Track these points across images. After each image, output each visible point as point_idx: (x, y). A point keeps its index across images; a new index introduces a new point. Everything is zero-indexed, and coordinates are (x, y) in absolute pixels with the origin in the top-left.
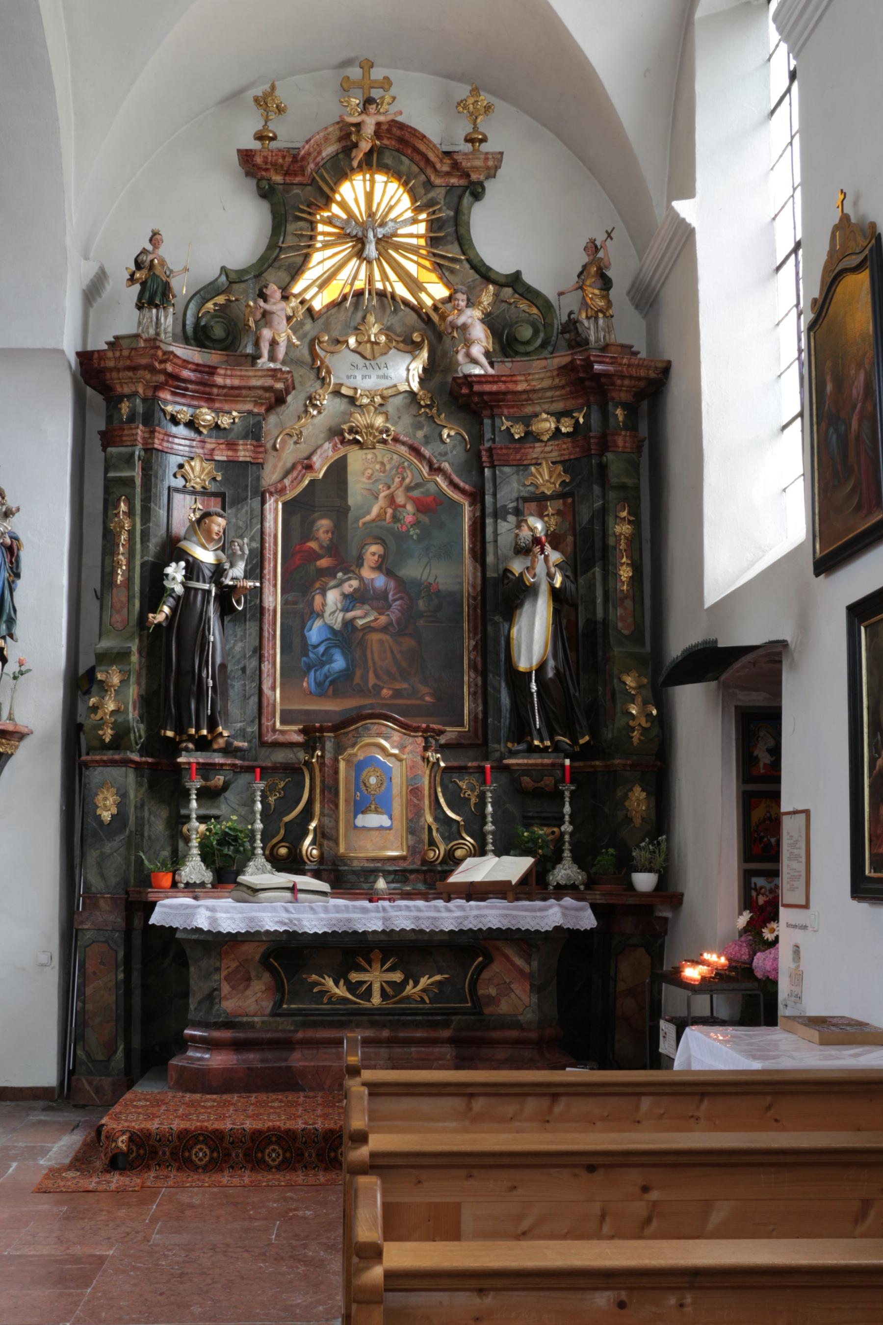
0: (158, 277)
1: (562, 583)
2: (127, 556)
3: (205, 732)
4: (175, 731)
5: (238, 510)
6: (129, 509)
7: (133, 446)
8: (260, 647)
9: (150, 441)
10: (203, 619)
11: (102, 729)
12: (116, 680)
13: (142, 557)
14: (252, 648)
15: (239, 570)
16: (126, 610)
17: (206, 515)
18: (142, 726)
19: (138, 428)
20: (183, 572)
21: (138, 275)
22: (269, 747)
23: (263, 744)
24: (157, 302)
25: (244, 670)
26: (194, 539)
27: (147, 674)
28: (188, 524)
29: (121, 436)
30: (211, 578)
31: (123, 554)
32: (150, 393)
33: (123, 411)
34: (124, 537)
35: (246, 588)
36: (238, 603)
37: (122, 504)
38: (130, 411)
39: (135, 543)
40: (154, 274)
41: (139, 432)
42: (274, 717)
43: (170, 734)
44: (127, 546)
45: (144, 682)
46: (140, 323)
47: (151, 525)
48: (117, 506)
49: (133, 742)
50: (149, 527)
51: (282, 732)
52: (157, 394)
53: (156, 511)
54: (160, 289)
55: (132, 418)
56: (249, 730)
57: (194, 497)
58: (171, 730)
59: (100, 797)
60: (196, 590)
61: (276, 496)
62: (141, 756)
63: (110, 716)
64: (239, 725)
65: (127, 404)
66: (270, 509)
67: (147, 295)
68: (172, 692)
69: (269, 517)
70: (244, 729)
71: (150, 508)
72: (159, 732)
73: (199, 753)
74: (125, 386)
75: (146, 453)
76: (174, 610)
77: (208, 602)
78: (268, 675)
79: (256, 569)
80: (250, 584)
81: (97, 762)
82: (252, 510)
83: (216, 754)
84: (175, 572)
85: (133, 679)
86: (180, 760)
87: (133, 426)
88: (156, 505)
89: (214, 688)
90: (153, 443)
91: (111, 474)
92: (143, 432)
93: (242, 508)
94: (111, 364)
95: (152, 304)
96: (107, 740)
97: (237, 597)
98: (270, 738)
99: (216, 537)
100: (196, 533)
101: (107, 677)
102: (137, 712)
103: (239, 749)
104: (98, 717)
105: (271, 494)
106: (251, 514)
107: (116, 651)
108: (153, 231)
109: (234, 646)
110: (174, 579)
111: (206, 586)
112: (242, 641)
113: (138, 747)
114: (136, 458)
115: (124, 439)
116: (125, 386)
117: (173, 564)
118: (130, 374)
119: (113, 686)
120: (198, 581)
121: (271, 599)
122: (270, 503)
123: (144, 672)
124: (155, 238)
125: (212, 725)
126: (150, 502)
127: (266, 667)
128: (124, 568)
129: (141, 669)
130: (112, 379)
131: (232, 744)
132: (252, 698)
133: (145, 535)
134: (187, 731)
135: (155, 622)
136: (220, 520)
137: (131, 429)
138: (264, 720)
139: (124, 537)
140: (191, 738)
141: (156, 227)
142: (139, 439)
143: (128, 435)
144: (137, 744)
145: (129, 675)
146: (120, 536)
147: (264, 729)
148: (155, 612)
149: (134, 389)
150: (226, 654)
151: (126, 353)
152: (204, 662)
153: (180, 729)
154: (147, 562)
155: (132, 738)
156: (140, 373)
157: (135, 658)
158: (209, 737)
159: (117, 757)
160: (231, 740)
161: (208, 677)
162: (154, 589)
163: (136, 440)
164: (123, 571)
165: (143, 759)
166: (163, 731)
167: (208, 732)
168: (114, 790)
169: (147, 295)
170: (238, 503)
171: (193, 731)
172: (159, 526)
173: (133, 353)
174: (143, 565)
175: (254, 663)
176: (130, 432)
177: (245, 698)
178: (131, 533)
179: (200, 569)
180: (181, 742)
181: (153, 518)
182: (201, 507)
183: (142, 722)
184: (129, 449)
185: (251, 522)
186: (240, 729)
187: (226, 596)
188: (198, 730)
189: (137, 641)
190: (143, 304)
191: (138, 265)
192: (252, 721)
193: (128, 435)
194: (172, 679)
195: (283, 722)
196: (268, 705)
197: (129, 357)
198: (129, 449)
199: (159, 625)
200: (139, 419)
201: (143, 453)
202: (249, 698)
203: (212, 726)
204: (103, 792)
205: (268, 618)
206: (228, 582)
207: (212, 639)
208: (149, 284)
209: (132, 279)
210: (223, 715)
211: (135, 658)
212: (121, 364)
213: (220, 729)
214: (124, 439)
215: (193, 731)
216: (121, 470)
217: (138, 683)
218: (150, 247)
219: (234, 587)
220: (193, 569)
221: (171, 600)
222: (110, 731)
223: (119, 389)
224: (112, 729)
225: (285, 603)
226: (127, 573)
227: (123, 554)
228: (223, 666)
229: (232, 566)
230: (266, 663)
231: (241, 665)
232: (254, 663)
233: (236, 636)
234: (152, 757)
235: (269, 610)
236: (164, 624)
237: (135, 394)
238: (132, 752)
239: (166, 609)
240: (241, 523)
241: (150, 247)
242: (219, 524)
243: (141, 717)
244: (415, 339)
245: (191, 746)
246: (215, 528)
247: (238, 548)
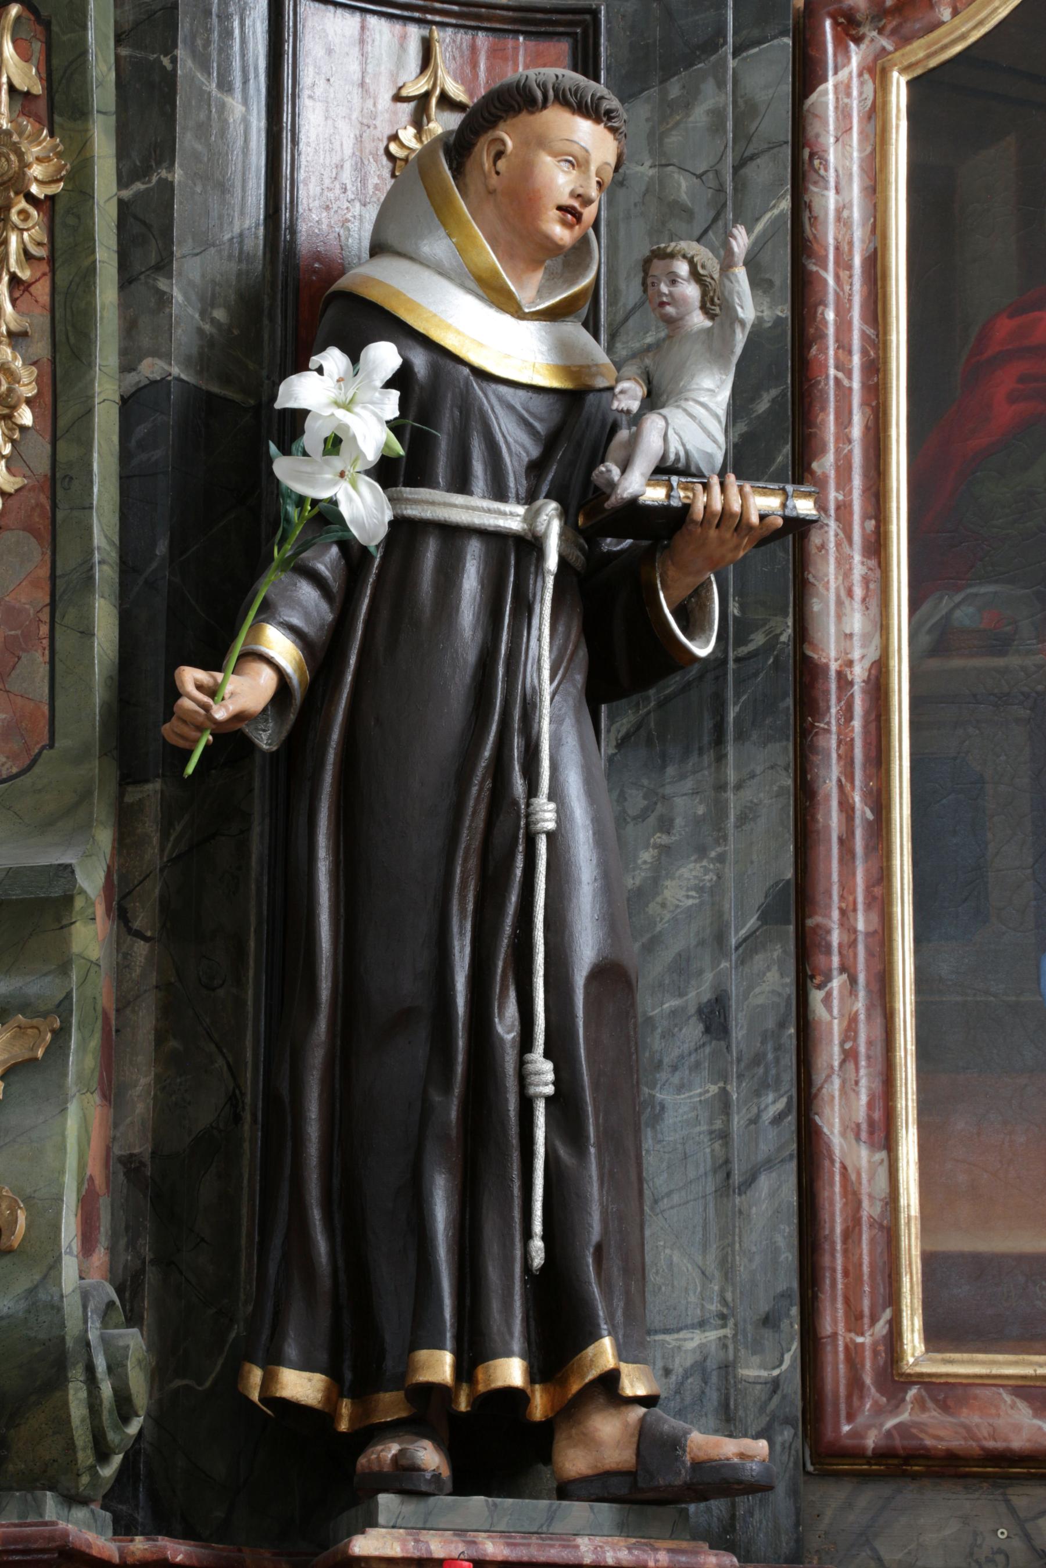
2: (41, 348)
3: (512, 1371)
4: (333, 1372)
5: (668, 111)
6: (49, 78)
8: (797, 902)
10: (492, 690)
13: (127, 367)
14: (757, 898)
15: (698, 420)
16: (40, 658)
17: (509, 102)
18: (134, 1341)
20: (391, 404)
22: (864, 1477)
23: (825, 1457)
25: (715, 1018)
26: (438, 246)
27: (160, 1039)
28: (379, 177)
30: (536, 469)
35: (741, 525)
36: (691, 617)
42: (893, 1299)
43: (301, 1385)
44: (42, 290)
45: (142, 1081)
47: (178, 175)
49: (81, 1436)
50: (167, 187)
51: (943, 1392)
53: (206, 99)
56: (752, 1371)
57: (414, 33)
58: (306, 1366)
60: (453, 534)
61: (877, 40)
62: (123, 1528)
64: (693, 1341)
66: (844, 113)
68: (313, 1131)
69: (841, 156)
70: (727, 1368)
71: (170, 79)
72: (234, 1376)
73: (478, 1501)
76: (323, 654)
77: (524, 608)
78: (849, 1056)
79: (778, 428)
80: (764, 503)
82: (746, 112)
83: (578, 1511)
84: (344, 399)
85: (81, 1058)
86: (365, 1545)
88: (205, 66)
89: (565, 1103)
93: (687, 104)
97: (684, 587)
98: (870, 1424)
99: (560, 233)
100: (442, 211)
102: (100, 1257)
103: (718, 1482)
105: (850, 28)
106: (742, 135)
109: (655, 882)
110: (334, 444)
111: (510, 518)
112: (702, 851)
113: (108, 1471)
117: (333, 359)
120: (461, 484)
121: (857, 622)
122: (843, 79)
123: (145, 1021)
125: (558, 1329)
126: (169, 47)
127: (835, 1006)
128: (26, 416)
129: (124, 1004)
131: (674, 1444)
132: (765, 1183)
133: (148, 235)
134: (407, 1366)
135: (220, 714)
136: (585, 132)
138: (833, 1320)
140: (428, 1410)
144: (103, 1455)
145: (61, 1035)
147: (835, 1372)
148: (213, 660)
150: (624, 907)
152: (503, 956)
153: (360, 1359)
154: (159, 386)
157: (90, 937)
158: (539, 1407)
160: (669, 1422)
161: (526, 1043)
162: (212, 499)
165: (139, 1546)
166: (256, 1375)
167: (533, 1375)
170: (668, 72)
171: (440, 1366)
172: (223, 188)
174: (131, 406)
175: (771, 979)
177: (730, 1182)
179: (470, 419)
180: (368, 1434)
181: (186, 140)
182: (456, 91)
183: (132, 1319)
185: (740, 185)
186: (700, 1368)
187: (623, 580)
188: (472, 1355)
189: (105, 837)
192: (769, 1321)
194: (316, 1058)
195: (936, 1336)
196: (851, 1233)
199: (232, 740)
202: (750, 1180)
203: (557, 1341)
205: (840, 729)
206: (638, 485)
207: (546, 816)
210: (614, 1266)
211: (90, 937)
213: (605, 1353)
215: (440, 1366)
217: (112, 1091)
219: (673, 520)
220: (437, 403)
221: (307, 592)
225: (933, 644)
226: (40, 450)
228: (610, 976)
229: (653, 401)
230: (837, 983)
231: (701, 991)
232: (773, 977)
233: (665, 825)
234: (188, 1534)
235: (844, 682)
236: (265, 740)
238: (72, 1499)
239: (280, 646)
240: (683, 186)
242: (575, 154)
243: (129, 1287)
245: (429, 1456)
246: (560, 182)
247: (691, 291)
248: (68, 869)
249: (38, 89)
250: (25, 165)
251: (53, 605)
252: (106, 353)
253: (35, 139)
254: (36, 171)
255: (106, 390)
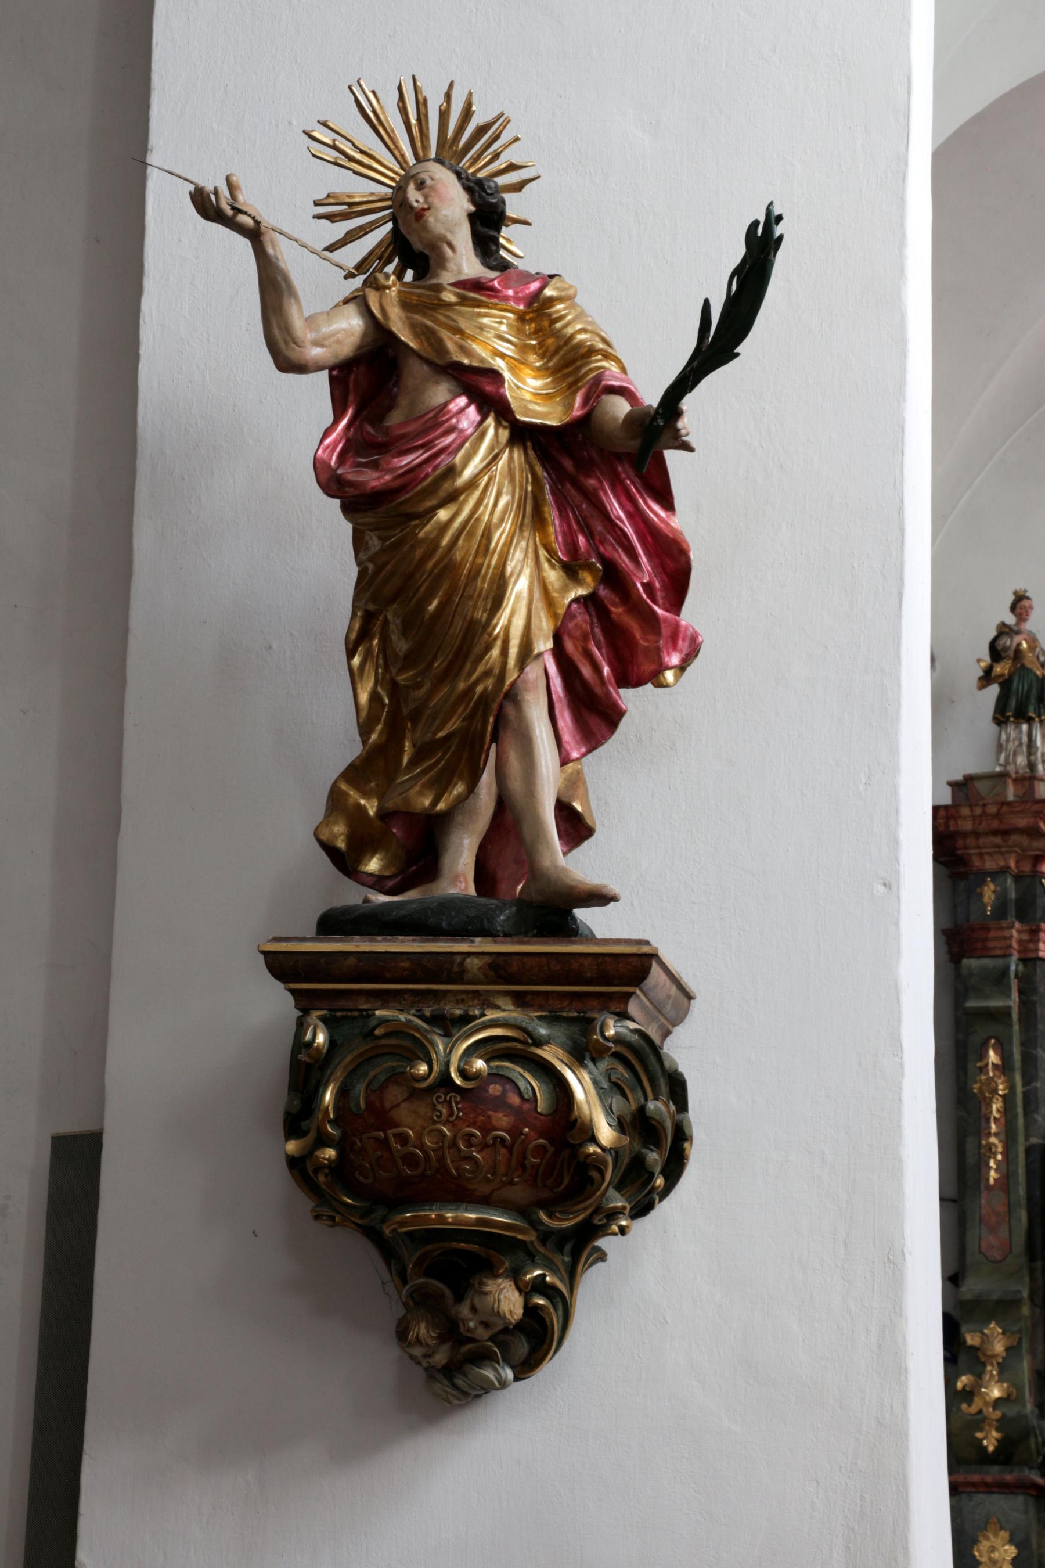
0: (1030, 671)
1: (1017, 892)
2: (1003, 1137)
6: (1003, 1059)
7: (1005, 956)
9: (1031, 946)
11: (981, 1430)
12: (999, 1347)
13: (1027, 1138)
16: (1006, 1227)
19: (1012, 927)
21: (998, 669)
24: (1031, 714)
29: (985, 940)
31: (996, 1135)
32: (1027, 868)
33: (986, 900)
34: (996, 1106)
37: (991, 1053)
38: (997, 898)
39: (1016, 1116)
40: (1023, 666)
41: (1015, 933)
44: (1003, 1120)
46: (1000, 748)
48: (983, 1056)
52: (1039, 869)
54: (1034, 692)
55: (1001, 910)
59: (984, 1545)
63: (994, 1409)
65: (992, 887)
67: (1013, 703)
74: (987, 858)
75: (1025, 966)
81: (974, 1485)
87: (1004, 924)
90: (1037, 950)
91: (972, 1003)
92: (1019, 932)
94: (967, 826)
95: (1021, 715)
96: (991, 1448)
101: (983, 1342)
104: (973, 1409)
107: (995, 1297)
108: (1015, 593)
114: (1012, 975)
115: (990, 944)
116: (987, 858)
118: (998, 840)
119: (994, 1356)
124: (1020, 603)
128: (999, 1157)
130: (966, 848)
137: (1002, 929)
139: (996, 1106)
141: (1020, 586)
142: (1015, 945)
143: (996, 939)
145: (1020, 1339)
146: (989, 1105)
149: (1002, 864)
151: (992, 809)
155: (1033, 1445)
156: (1014, 838)
157: (1025, 1310)
159: (1009, 1477)
163: (1010, 947)
164: (997, 1162)
168: (1004, 1534)
169: (1013, 703)
173: (1005, 809)
174: (1028, 1151)
176: (1000, 933)
178: (1008, 1100)
184: (1000, 962)
189: (1027, 1279)
190: (1008, 717)
191: (996, 652)
193: (996, 939)
197: (998, 816)
198: (1000, 962)
200: (1012, 911)
201: (1021, 968)
204: (987, 1538)
208: (1015, 684)
209: (987, 678)
211: (1025, 1310)
212: (983, 827)
214: (990, 944)
216: (987, 997)
217: (1032, 1352)
218: (1010, 620)
222: (994, 1434)
223: (977, 863)
224: (997, 1430)
226: (1004, 1168)
227: (996, 1135)
237: (1004, 870)
238: (1031, 1468)
241: (1010, 620)
244: (994, 1329)
248: (1019, 1292)
249: (1000, 1063)
250: (997, 1085)
251: (1009, 1212)
252: (1021, 1138)
253: (1000, 1078)
254: (1001, 1087)
255: (1021, 1149)
